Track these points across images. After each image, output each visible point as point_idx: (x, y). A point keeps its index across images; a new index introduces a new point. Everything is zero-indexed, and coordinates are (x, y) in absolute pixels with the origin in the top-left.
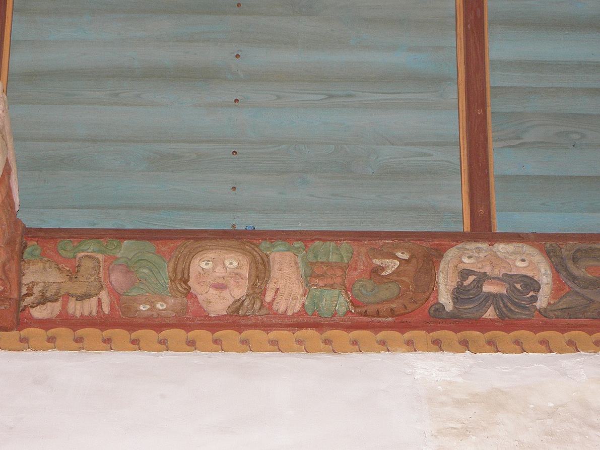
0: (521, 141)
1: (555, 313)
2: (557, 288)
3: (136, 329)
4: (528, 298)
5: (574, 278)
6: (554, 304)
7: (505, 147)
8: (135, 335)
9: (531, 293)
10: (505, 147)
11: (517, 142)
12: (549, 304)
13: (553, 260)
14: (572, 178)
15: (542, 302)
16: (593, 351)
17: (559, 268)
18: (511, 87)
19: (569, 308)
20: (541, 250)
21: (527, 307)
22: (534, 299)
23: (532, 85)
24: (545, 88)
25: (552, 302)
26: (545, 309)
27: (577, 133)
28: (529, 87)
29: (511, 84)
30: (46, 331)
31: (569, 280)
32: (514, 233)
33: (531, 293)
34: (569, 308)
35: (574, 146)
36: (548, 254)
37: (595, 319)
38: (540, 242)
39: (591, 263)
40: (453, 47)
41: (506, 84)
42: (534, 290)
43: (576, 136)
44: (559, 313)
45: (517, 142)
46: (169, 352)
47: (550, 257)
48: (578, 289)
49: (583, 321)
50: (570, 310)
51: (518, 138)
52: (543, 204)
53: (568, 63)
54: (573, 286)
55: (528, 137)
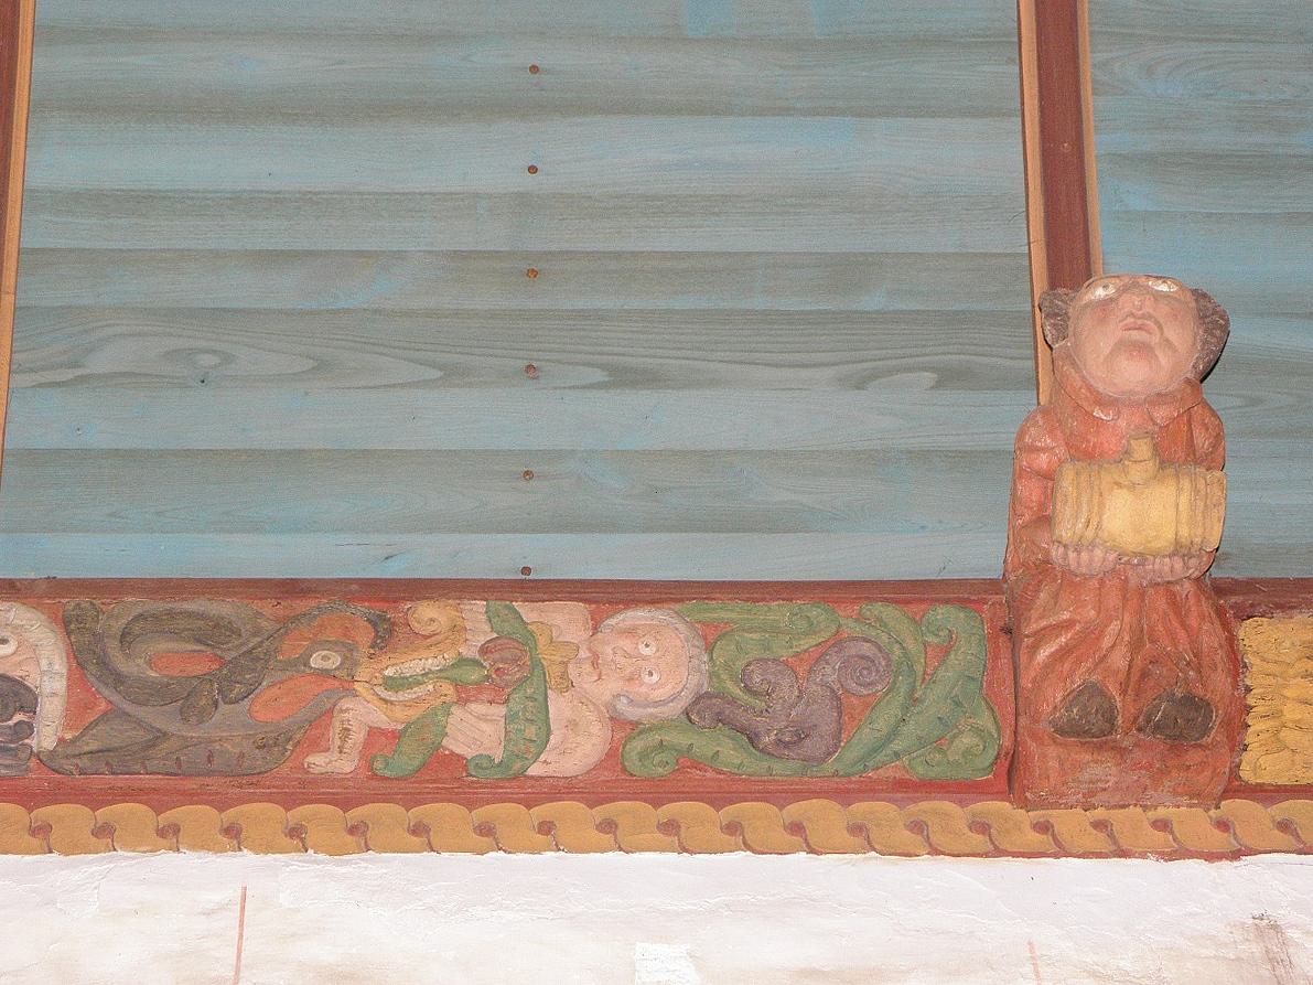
0: (79, 372)
1: (78, 762)
2: (77, 708)
3: (607, 775)
4: (10, 727)
5: (118, 680)
6: (74, 741)
7: (41, 385)
8: (104, 813)
9: (18, 717)
10: (41, 385)
11: (69, 375)
12: (61, 741)
13: (73, 640)
14: (188, 453)
15: (46, 737)
16: (149, 848)
17: (87, 659)
18: (71, 250)
19: (109, 750)
20: (53, 618)
21: (11, 749)
22: (27, 729)
23: (120, 245)
24: (151, 250)
25: (68, 736)
26: (52, 753)
27: (214, 352)
28: (112, 250)
29: (73, 244)
30: (94, 810)
31: (106, 684)
32: (242, 579)
33: (18, 717)
34: (109, 750)
35: (203, 382)
36: (67, 625)
37: (171, 774)
38: (57, 600)
39: (163, 646)
40: (1023, 254)
41: (62, 243)
42: (21, 709)
43: (208, 360)
44: (84, 762)
45: (69, 375)
46: (54, 857)
47: (69, 634)
48: (127, 707)
49: (146, 780)
50: (112, 754)
51: (75, 365)
52: (112, 515)
53: (210, 196)
54: (115, 698)
55: (99, 364)
